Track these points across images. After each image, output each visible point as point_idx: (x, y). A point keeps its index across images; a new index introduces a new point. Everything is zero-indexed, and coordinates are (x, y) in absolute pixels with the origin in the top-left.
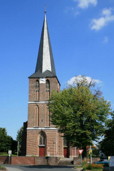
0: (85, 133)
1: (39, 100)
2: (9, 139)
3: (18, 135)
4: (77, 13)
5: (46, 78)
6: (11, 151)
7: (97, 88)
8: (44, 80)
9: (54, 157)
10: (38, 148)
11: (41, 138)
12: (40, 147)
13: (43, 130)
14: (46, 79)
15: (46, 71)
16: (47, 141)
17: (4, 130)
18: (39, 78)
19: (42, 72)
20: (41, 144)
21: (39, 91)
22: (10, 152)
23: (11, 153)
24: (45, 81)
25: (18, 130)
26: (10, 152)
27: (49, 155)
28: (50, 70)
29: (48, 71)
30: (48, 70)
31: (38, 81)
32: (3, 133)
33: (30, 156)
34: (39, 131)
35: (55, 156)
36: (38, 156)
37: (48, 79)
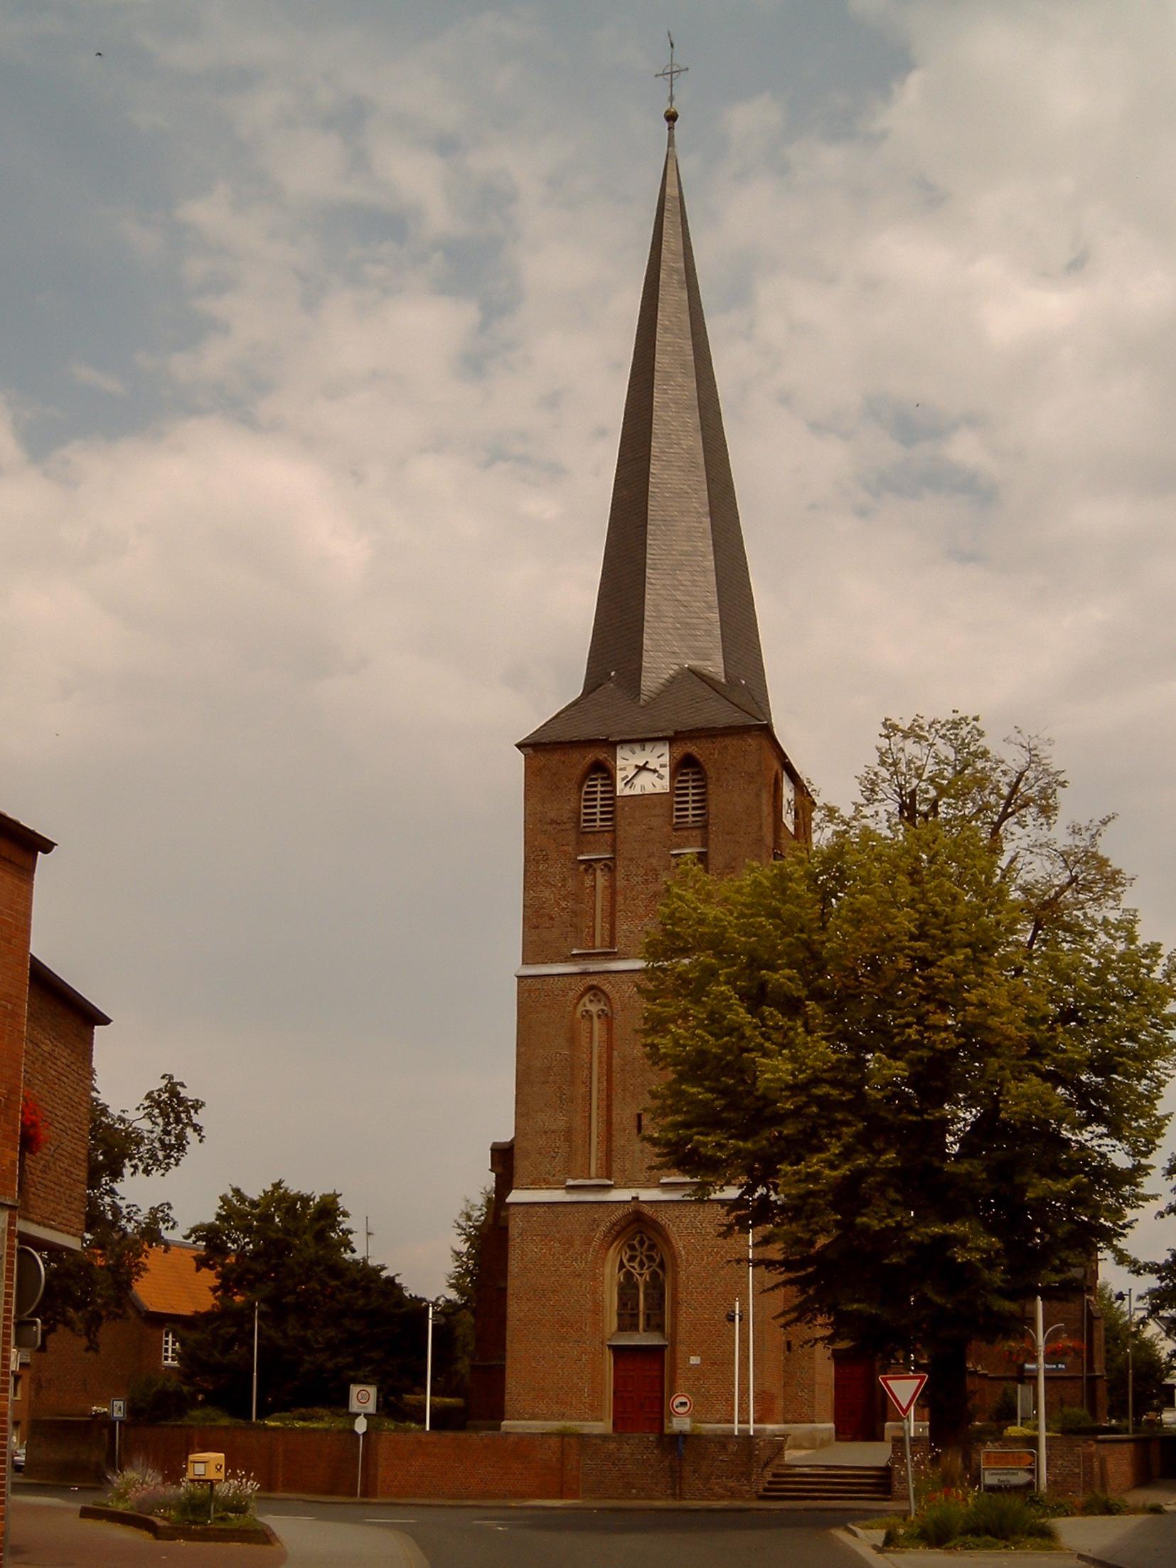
0: (946, 1241)
1: (612, 945)
2: (367, 1291)
3: (464, 1248)
4: (840, 1026)
5: (672, 740)
6: (372, 1391)
7: (1076, 831)
8: (659, 757)
9: (729, 1436)
10: (609, 1358)
11: (629, 1275)
12: (620, 1352)
13: (647, 1210)
14: (681, 750)
15: (673, 680)
16: (683, 1308)
17: (328, 1211)
18: (611, 746)
19: (650, 660)
20: (627, 1321)
21: (610, 866)
22: (363, 1398)
23: (371, 1408)
24: (666, 772)
25: (462, 1206)
26: (363, 1398)
27: (680, 1423)
28: (715, 666)
29: (697, 675)
30: (692, 671)
31: (605, 771)
32: (321, 1236)
33: (536, 1426)
34: (619, 1213)
35: (736, 1427)
36: (603, 1426)
37: (692, 749)
